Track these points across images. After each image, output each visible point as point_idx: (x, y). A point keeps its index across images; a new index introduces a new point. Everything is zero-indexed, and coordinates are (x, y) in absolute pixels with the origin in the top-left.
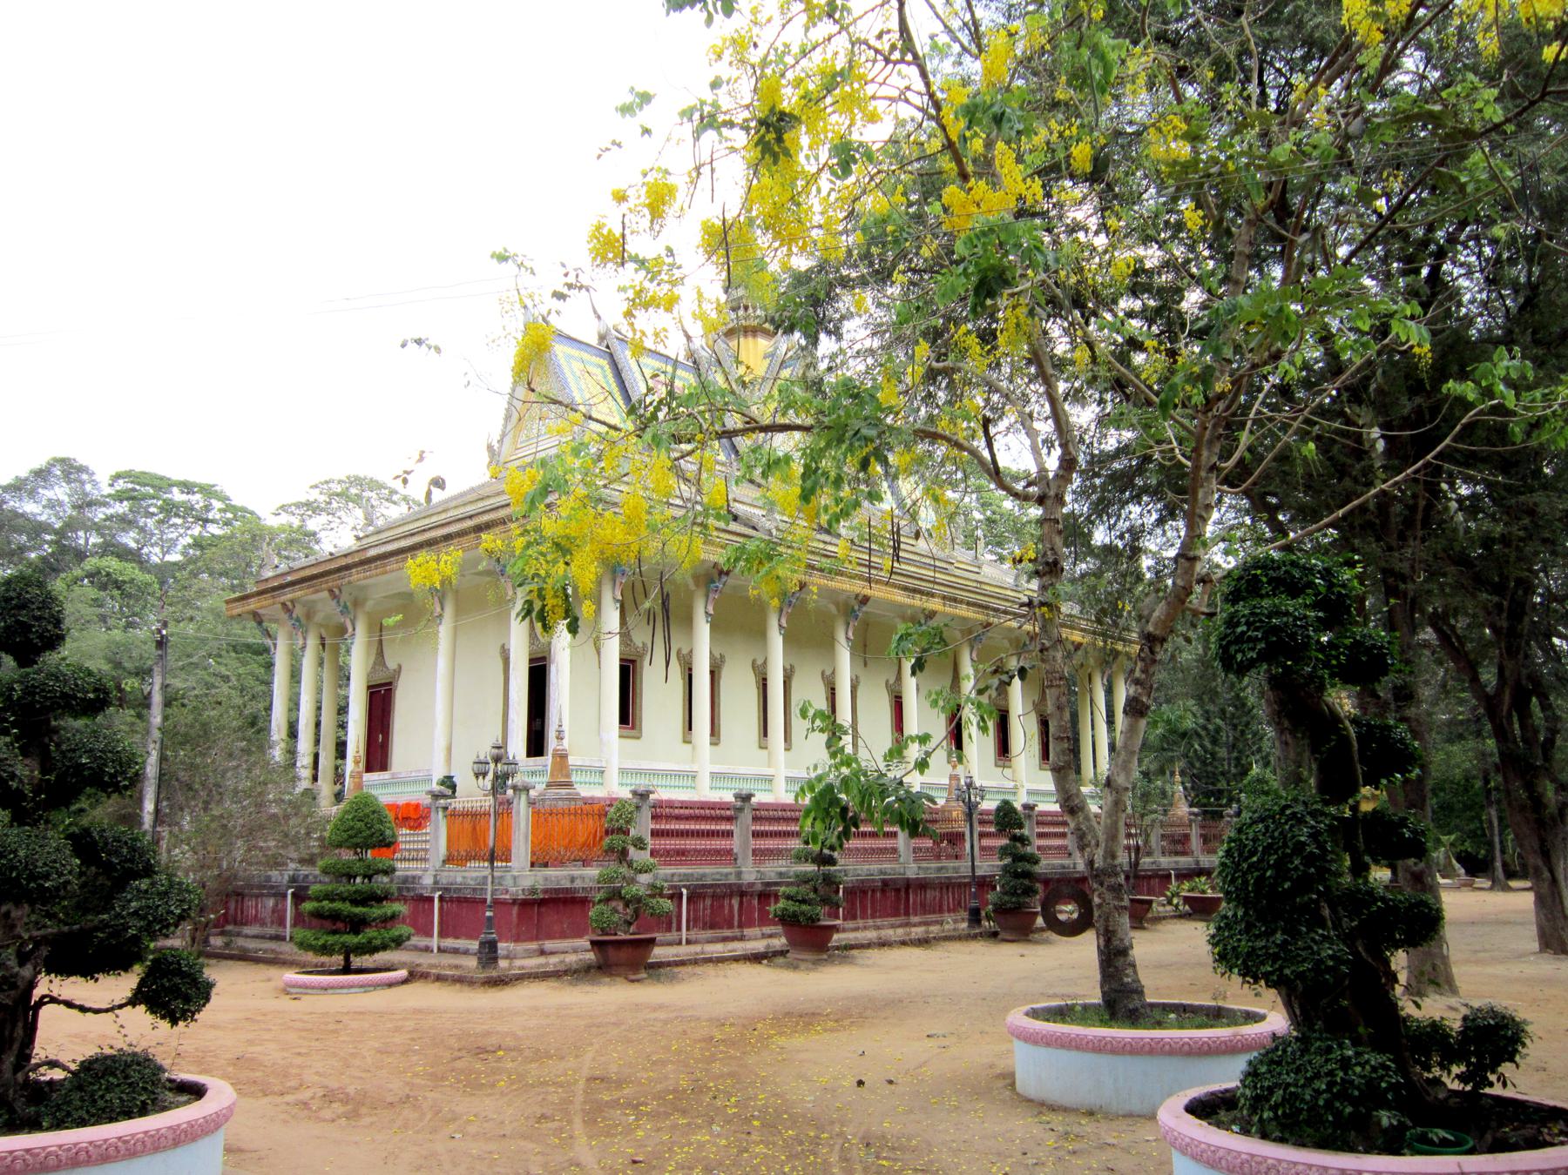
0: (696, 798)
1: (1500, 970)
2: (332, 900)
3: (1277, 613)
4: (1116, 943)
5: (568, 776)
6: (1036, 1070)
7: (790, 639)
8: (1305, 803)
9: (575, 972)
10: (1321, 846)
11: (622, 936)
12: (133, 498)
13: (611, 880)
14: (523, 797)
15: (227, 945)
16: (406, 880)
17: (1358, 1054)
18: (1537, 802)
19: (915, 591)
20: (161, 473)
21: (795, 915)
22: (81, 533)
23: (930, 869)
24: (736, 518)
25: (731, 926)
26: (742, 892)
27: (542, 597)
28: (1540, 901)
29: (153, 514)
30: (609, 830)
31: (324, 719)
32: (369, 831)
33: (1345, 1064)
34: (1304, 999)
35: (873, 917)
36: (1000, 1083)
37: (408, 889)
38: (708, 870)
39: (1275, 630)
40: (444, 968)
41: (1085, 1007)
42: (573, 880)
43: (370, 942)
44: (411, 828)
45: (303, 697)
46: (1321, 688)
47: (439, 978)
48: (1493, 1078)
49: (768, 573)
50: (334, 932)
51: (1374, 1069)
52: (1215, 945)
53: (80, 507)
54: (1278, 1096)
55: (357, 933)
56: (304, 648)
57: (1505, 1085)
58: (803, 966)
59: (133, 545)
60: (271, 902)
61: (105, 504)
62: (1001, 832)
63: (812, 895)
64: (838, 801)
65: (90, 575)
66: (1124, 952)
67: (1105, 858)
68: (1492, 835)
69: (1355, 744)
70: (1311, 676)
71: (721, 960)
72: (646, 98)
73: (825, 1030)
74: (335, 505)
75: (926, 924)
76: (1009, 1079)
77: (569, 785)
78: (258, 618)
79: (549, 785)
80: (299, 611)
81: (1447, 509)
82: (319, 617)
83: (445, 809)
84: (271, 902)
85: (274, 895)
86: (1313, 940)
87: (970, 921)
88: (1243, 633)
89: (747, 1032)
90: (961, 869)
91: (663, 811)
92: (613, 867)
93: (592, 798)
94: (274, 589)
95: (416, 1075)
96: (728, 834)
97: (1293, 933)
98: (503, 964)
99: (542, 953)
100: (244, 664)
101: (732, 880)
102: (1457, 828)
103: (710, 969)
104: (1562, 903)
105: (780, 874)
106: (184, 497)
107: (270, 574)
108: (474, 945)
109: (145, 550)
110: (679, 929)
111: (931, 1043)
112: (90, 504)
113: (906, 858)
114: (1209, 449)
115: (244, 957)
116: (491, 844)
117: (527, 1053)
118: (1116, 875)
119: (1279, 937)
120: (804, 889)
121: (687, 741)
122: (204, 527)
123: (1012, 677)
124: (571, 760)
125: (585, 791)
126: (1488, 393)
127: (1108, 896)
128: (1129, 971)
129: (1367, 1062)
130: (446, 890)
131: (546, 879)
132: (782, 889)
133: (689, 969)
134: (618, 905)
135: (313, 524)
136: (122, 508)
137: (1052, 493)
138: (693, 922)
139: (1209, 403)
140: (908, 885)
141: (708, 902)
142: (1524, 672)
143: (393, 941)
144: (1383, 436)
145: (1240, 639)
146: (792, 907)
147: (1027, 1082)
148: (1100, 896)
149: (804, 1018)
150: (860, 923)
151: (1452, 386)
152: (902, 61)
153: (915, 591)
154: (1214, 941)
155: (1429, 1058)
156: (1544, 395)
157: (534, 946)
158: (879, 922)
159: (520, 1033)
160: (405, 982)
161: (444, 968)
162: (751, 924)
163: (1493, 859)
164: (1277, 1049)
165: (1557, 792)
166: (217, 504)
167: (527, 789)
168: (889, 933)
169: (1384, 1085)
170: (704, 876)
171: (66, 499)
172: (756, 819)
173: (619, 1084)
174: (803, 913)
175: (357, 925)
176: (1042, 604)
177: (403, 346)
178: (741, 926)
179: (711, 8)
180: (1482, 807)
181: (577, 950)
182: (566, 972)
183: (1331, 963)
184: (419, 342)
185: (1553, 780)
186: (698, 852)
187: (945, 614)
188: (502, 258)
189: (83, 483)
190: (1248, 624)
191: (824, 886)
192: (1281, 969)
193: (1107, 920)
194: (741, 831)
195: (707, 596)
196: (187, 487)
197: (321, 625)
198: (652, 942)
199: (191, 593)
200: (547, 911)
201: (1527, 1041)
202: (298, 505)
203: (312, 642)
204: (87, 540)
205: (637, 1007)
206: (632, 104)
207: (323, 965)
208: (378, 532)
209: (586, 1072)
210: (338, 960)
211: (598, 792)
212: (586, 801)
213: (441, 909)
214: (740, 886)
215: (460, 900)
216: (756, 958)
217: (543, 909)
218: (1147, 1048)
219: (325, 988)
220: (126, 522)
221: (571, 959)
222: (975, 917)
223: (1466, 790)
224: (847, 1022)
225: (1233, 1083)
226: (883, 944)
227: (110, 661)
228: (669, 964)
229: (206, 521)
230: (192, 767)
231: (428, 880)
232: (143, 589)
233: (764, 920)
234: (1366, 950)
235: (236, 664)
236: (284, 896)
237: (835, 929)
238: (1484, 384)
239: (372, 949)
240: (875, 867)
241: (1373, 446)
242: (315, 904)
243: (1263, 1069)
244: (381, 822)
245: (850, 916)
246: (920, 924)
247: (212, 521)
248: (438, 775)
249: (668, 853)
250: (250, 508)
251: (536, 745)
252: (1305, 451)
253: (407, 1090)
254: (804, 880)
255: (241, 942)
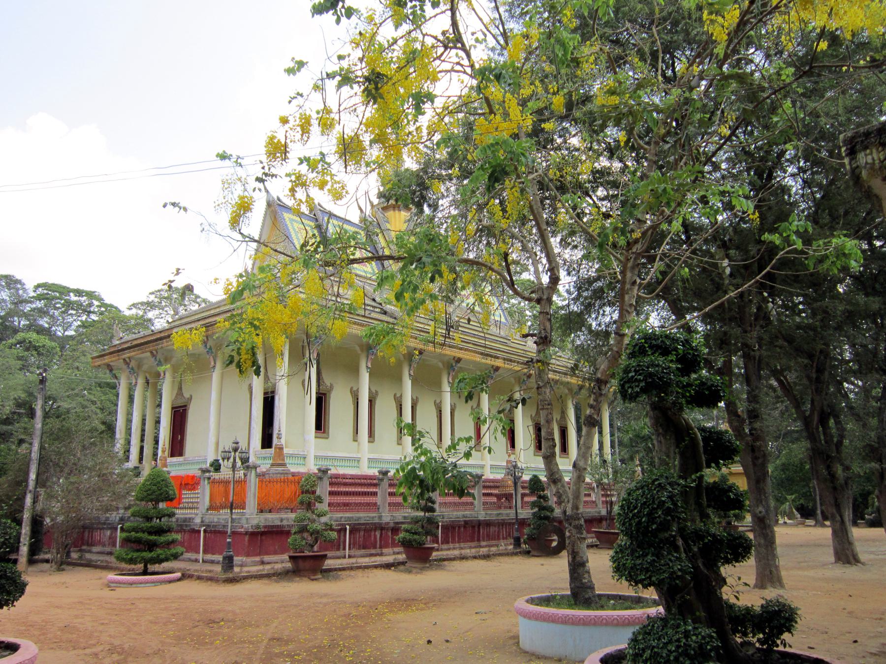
0: (359, 473)
1: (811, 573)
2: (137, 532)
3: (653, 365)
4: (578, 559)
5: (283, 460)
6: (533, 635)
7: (415, 381)
8: (667, 478)
9: (280, 574)
10: (675, 504)
11: (307, 553)
12: (47, 299)
13: (302, 520)
14: (253, 472)
15: (81, 558)
16: (185, 520)
17: (695, 628)
18: (833, 476)
19: (487, 355)
20: (64, 284)
21: (410, 541)
22: (16, 318)
23: (493, 515)
24: (385, 313)
25: (375, 547)
26: (382, 528)
27: (239, 354)
28: (834, 532)
29: (59, 308)
30: (305, 492)
31: (147, 427)
32: (159, 491)
33: (687, 634)
34: (670, 594)
35: (459, 542)
36: (511, 642)
37: (186, 526)
38: (362, 515)
39: (651, 375)
40: (202, 572)
41: (562, 597)
42: (282, 520)
43: (158, 556)
44: (189, 490)
45: (136, 415)
46: (681, 409)
47: (199, 578)
48: (779, 642)
49: (387, 343)
50: (138, 551)
51: (703, 638)
52: (614, 562)
53: (16, 303)
54: (648, 653)
55: (151, 551)
56: (136, 385)
57: (785, 646)
58: (415, 571)
59: (46, 326)
60: (108, 533)
61: (31, 302)
62: (532, 493)
63: (420, 530)
64: (418, 476)
65: (20, 343)
66: (583, 564)
67: (572, 509)
68: (816, 495)
69: (702, 444)
70: (674, 403)
71: (367, 567)
72: (301, 64)
73: (417, 610)
74: (163, 304)
75: (490, 546)
76: (516, 638)
77: (284, 465)
78: (110, 368)
79: (272, 465)
80: (133, 364)
81: (767, 307)
82: (145, 367)
83: (209, 478)
84: (108, 533)
85: (110, 528)
86: (670, 560)
87: (515, 545)
88: (633, 377)
89: (371, 611)
90: (508, 514)
91: (337, 481)
92: (300, 513)
93: (298, 473)
94: (119, 351)
95: (168, 636)
96: (375, 494)
97: (658, 555)
98: (236, 569)
99: (263, 563)
100: (105, 394)
101: (376, 521)
102: (796, 491)
103: (359, 573)
104: (847, 534)
105: (405, 517)
106: (76, 298)
107: (118, 342)
108: (219, 558)
109: (54, 328)
110: (344, 549)
111: (479, 617)
112: (22, 302)
113: (478, 509)
114: (632, 272)
115: (89, 565)
116: (231, 499)
117: (238, 623)
118: (579, 519)
119: (649, 558)
120: (415, 527)
121: (355, 440)
122: (88, 315)
123: (518, 404)
124: (285, 451)
125: (293, 469)
126: (787, 241)
127: (574, 531)
128: (586, 576)
129: (700, 633)
130: (208, 526)
131: (266, 520)
132: (403, 526)
133: (347, 573)
134: (305, 536)
135: (151, 315)
136: (39, 304)
137: (545, 297)
138: (352, 545)
139: (629, 245)
140: (480, 524)
141: (362, 533)
142: (825, 403)
143: (172, 555)
144: (729, 265)
145: (630, 380)
146: (408, 536)
147: (526, 643)
148: (569, 531)
149: (405, 602)
150: (451, 545)
151: (766, 236)
152: (455, 47)
153: (487, 355)
154: (614, 559)
155: (746, 629)
156: (824, 243)
157: (257, 559)
158: (462, 545)
159: (238, 611)
160: (179, 580)
161: (202, 572)
162: (387, 546)
163: (816, 508)
164: (649, 625)
165: (844, 471)
166: (96, 303)
167: (255, 467)
168: (467, 552)
169: (709, 647)
170: (359, 518)
171: (8, 298)
172: (331, 484)
173: (287, 642)
174: (415, 540)
175: (151, 546)
176: (538, 361)
177: (165, 206)
178: (381, 547)
179: (339, 13)
180: (810, 480)
181: (281, 561)
182: (274, 575)
183: (680, 573)
184: (174, 204)
185: (842, 464)
186: (356, 504)
187: (504, 368)
188: (223, 157)
189: (18, 289)
190: (635, 371)
191: (425, 522)
192: (650, 577)
193: (573, 546)
194: (382, 491)
195: (368, 357)
196: (79, 293)
197: (146, 372)
198: (325, 557)
199: (77, 354)
200: (265, 538)
201: (798, 620)
202: (142, 304)
203: (141, 381)
204: (19, 322)
205: (312, 595)
206: (293, 68)
207: (133, 570)
208: (181, 319)
209: (269, 635)
210: (141, 566)
211: (302, 470)
212: (293, 474)
213: (205, 537)
214: (381, 524)
215: (215, 532)
216: (388, 566)
217: (264, 537)
218: (593, 621)
219: (131, 584)
220: (42, 312)
221: (278, 567)
222: (517, 542)
223: (801, 470)
224: (431, 605)
225: (623, 646)
226: (463, 558)
227: (26, 392)
228: (336, 570)
229: (90, 312)
230: (60, 454)
231: (198, 520)
232: (50, 353)
233: (394, 545)
234: (704, 564)
235: (99, 394)
236: (116, 529)
237: (432, 549)
238: (785, 235)
239: (160, 561)
240: (460, 513)
241: (724, 271)
242: (128, 534)
243: (640, 637)
244: (167, 487)
245: (446, 541)
246: (486, 546)
247: (94, 312)
248: (210, 459)
249: (338, 505)
250: (115, 305)
251: (267, 442)
252: (682, 273)
253: (160, 646)
254: (416, 521)
255: (88, 556)
